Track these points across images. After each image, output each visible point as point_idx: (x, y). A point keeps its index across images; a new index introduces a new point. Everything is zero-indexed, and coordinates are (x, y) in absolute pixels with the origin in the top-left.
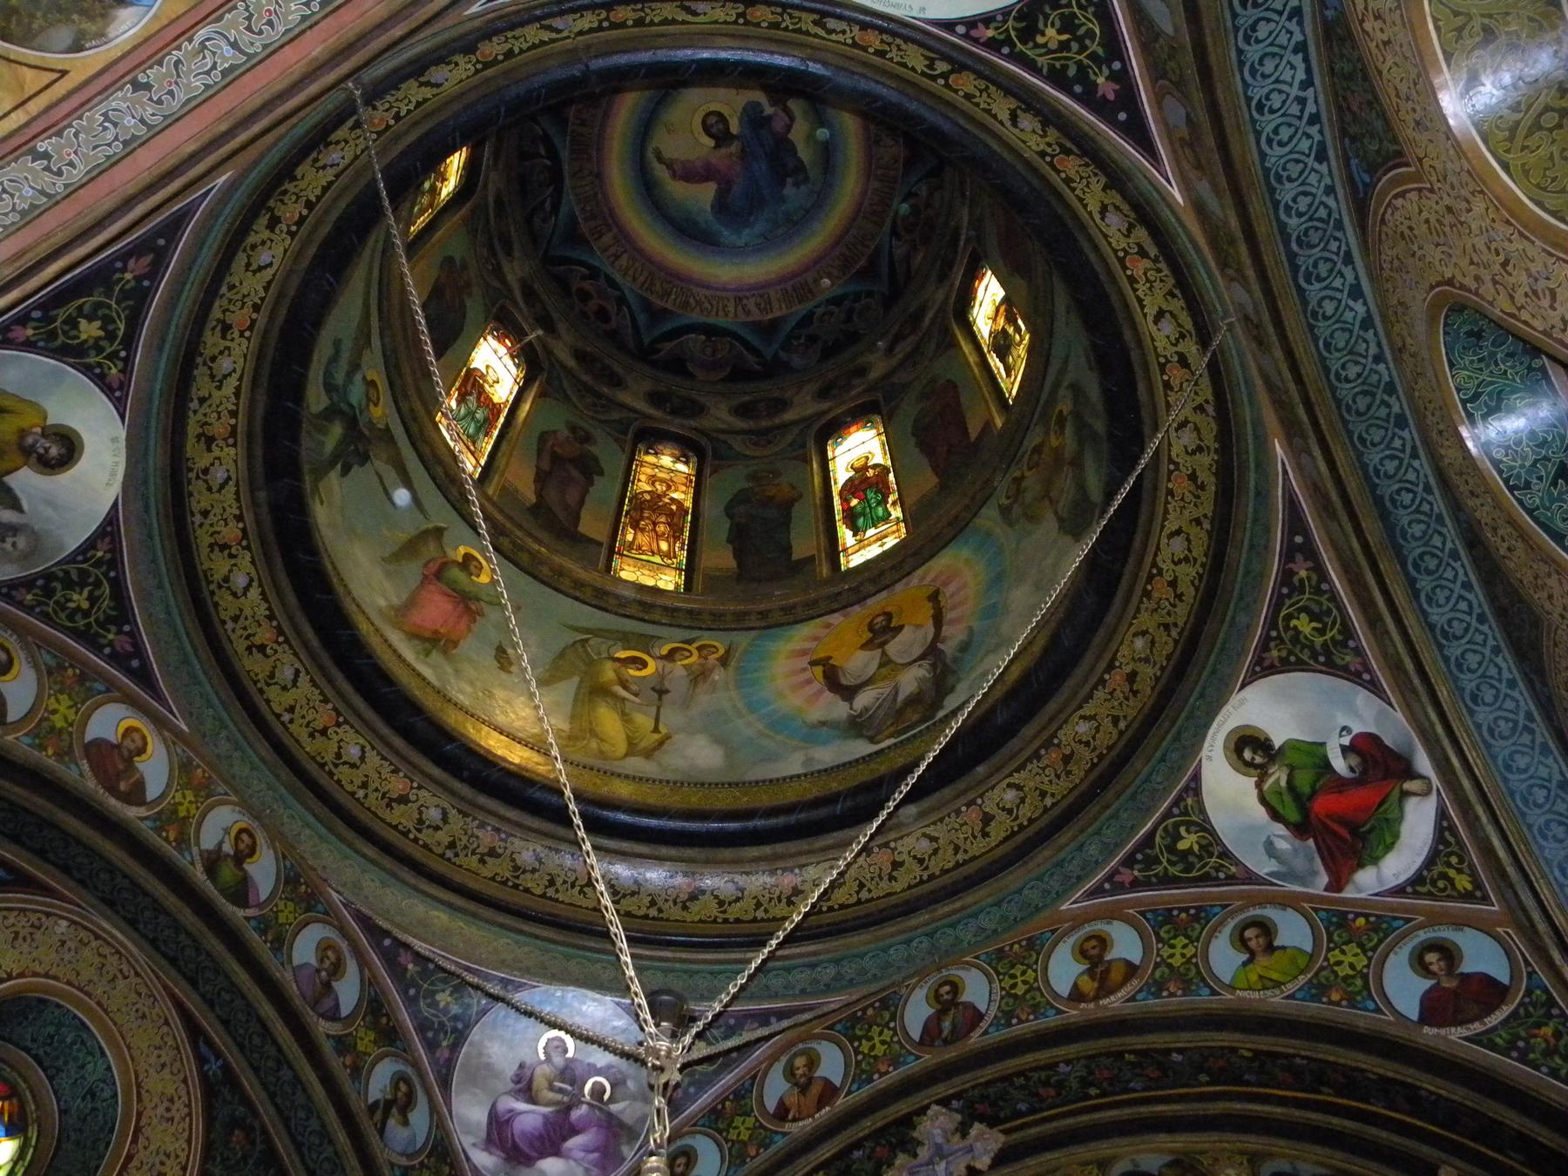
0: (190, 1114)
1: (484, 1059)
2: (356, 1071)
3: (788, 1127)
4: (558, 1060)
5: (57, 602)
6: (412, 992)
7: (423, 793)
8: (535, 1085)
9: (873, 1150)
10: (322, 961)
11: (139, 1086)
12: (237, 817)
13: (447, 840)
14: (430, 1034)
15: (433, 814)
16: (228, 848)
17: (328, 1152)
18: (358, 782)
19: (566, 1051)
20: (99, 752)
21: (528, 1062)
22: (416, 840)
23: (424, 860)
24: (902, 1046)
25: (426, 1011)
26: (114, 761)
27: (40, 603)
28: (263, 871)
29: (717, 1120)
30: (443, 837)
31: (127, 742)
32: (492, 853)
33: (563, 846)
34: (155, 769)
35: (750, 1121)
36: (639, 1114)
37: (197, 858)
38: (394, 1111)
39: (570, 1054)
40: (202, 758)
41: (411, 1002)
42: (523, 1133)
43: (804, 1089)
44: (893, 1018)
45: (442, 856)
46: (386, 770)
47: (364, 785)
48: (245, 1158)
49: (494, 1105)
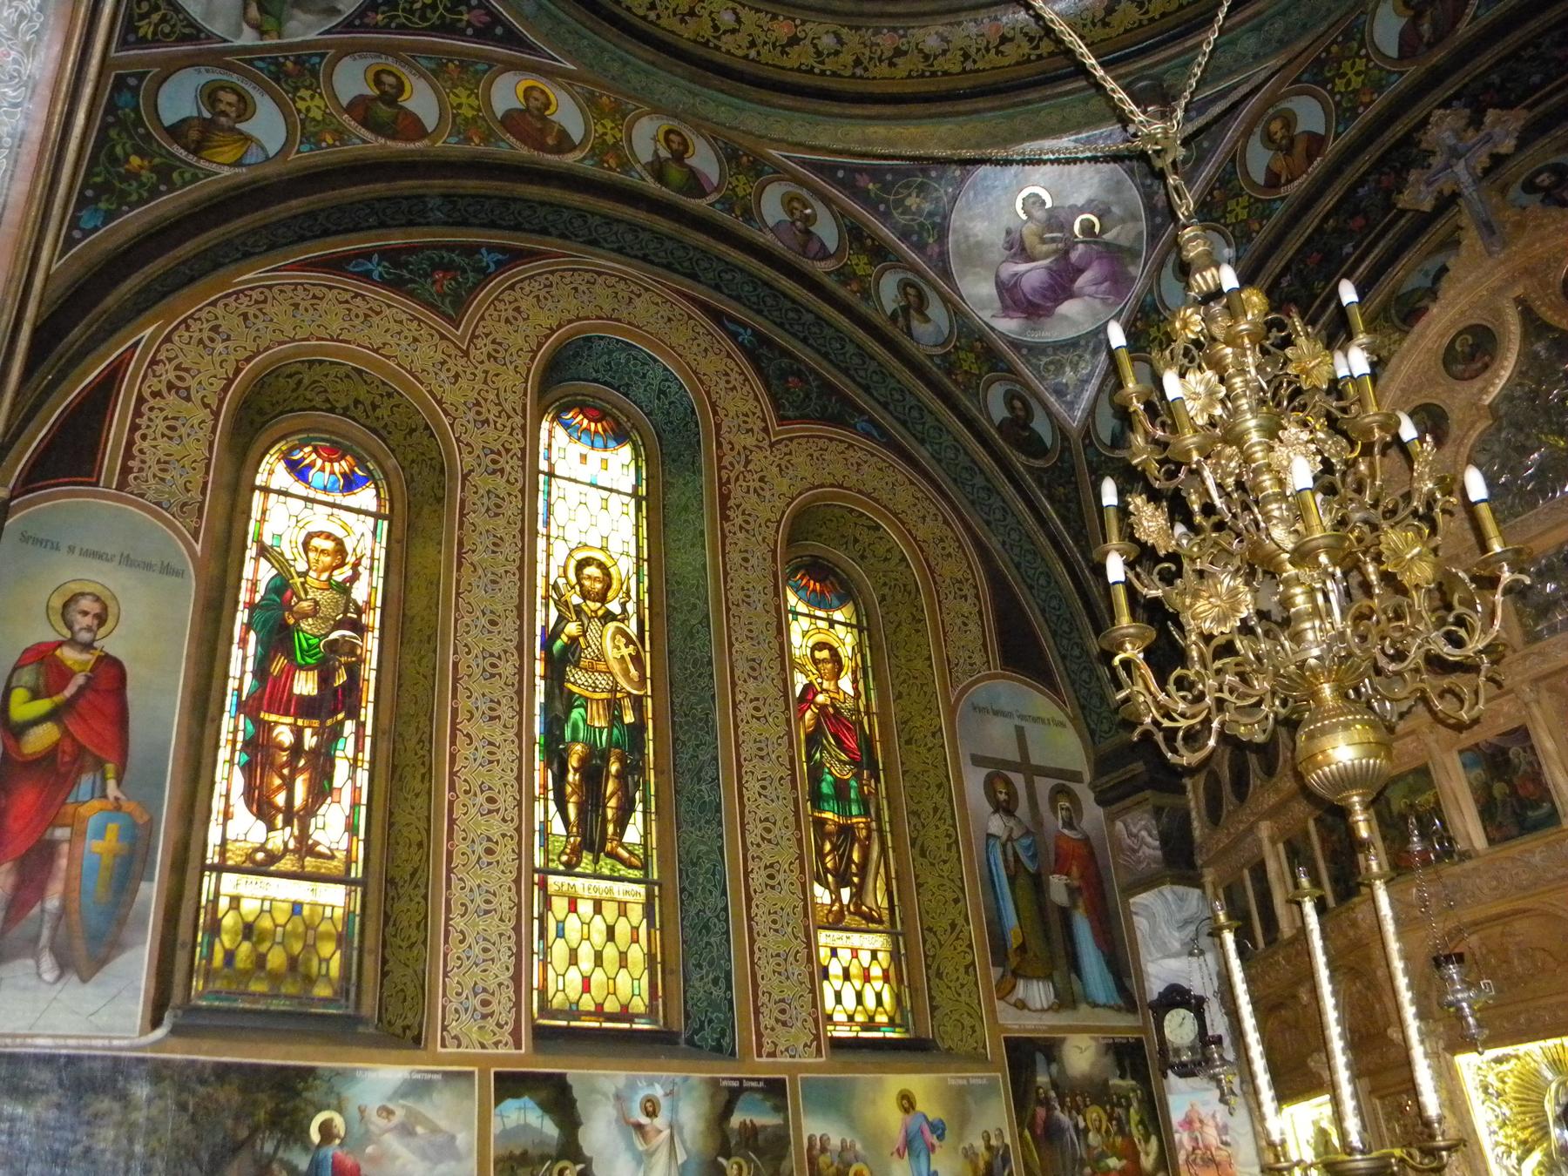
0: (746, 379)
1: (972, 240)
2: (866, 295)
3: (1283, 191)
4: (1039, 214)
5: (404, 10)
6: (882, 207)
7: (808, 26)
8: (1027, 244)
9: (1379, 182)
10: (792, 214)
11: (695, 372)
12: (657, 123)
13: (850, 59)
14: (915, 238)
15: (827, 42)
16: (664, 153)
17: (873, 366)
18: (745, 44)
19: (1044, 203)
20: (511, 121)
21: (1012, 226)
22: (823, 73)
23: (839, 87)
24: (1381, 69)
25: (902, 220)
26: (529, 122)
27: (392, 18)
28: (704, 159)
29: (1210, 212)
30: (847, 58)
31: (533, 103)
32: (899, 52)
33: (963, 16)
34: (567, 114)
35: (1244, 201)
36: (1133, 234)
37: (645, 174)
38: (912, 312)
39: (1049, 205)
40: (602, 87)
41: (885, 217)
42: (1034, 290)
43: (1288, 150)
44: (1362, 45)
45: (853, 76)
46: (764, 19)
47: (753, 44)
48: (807, 396)
49: (997, 276)
